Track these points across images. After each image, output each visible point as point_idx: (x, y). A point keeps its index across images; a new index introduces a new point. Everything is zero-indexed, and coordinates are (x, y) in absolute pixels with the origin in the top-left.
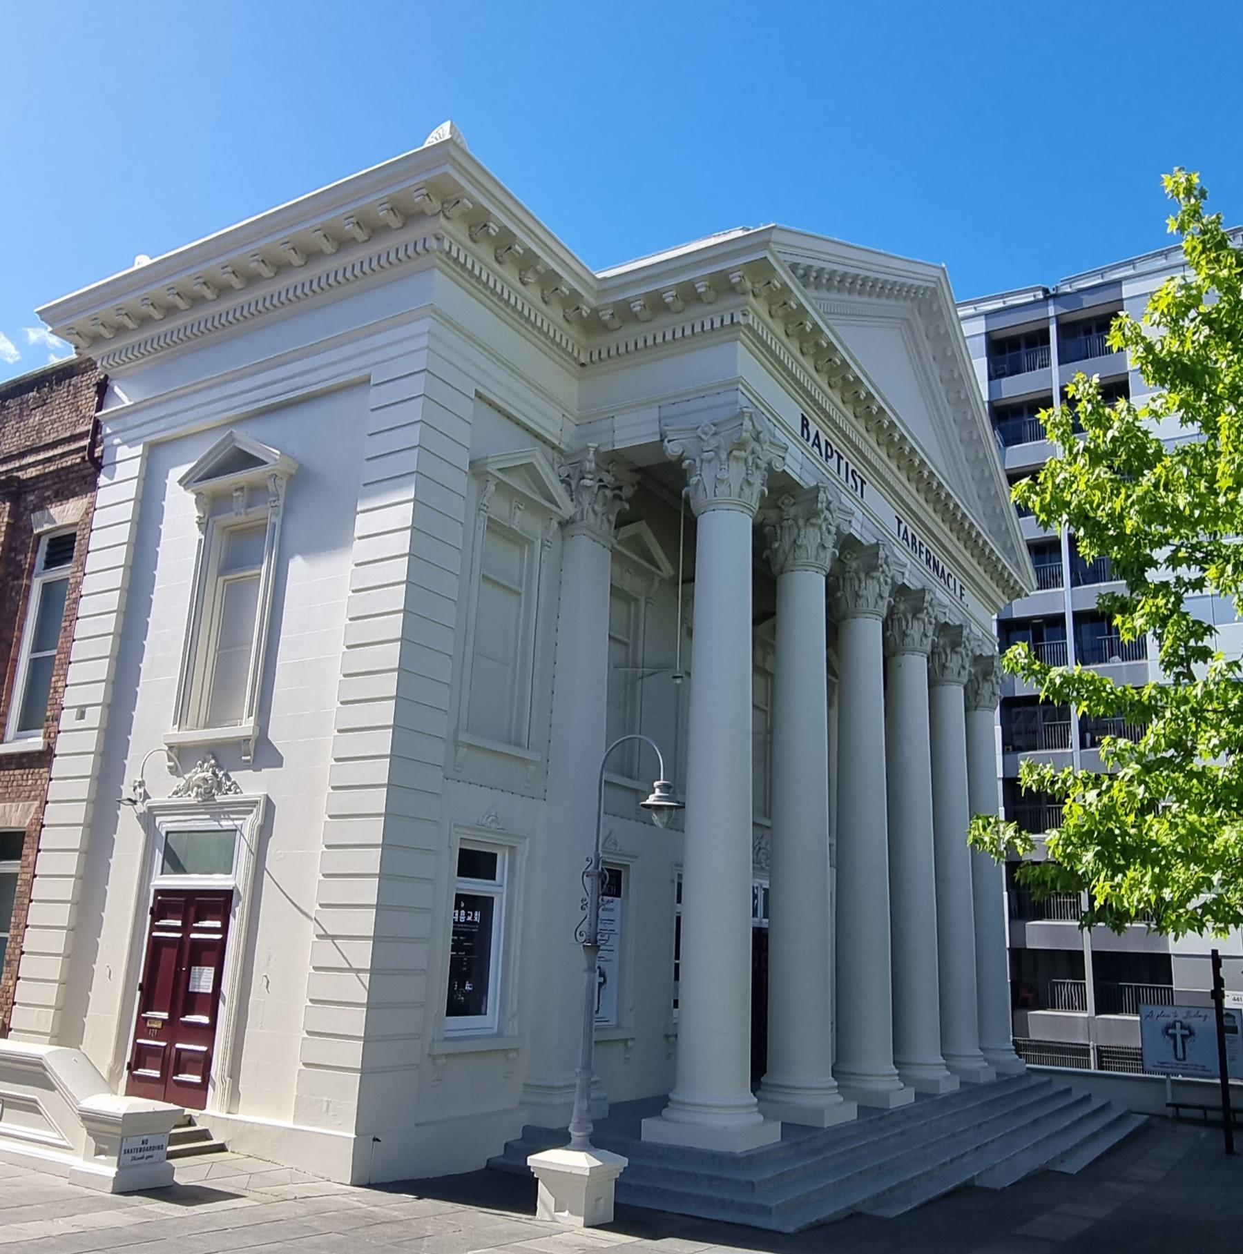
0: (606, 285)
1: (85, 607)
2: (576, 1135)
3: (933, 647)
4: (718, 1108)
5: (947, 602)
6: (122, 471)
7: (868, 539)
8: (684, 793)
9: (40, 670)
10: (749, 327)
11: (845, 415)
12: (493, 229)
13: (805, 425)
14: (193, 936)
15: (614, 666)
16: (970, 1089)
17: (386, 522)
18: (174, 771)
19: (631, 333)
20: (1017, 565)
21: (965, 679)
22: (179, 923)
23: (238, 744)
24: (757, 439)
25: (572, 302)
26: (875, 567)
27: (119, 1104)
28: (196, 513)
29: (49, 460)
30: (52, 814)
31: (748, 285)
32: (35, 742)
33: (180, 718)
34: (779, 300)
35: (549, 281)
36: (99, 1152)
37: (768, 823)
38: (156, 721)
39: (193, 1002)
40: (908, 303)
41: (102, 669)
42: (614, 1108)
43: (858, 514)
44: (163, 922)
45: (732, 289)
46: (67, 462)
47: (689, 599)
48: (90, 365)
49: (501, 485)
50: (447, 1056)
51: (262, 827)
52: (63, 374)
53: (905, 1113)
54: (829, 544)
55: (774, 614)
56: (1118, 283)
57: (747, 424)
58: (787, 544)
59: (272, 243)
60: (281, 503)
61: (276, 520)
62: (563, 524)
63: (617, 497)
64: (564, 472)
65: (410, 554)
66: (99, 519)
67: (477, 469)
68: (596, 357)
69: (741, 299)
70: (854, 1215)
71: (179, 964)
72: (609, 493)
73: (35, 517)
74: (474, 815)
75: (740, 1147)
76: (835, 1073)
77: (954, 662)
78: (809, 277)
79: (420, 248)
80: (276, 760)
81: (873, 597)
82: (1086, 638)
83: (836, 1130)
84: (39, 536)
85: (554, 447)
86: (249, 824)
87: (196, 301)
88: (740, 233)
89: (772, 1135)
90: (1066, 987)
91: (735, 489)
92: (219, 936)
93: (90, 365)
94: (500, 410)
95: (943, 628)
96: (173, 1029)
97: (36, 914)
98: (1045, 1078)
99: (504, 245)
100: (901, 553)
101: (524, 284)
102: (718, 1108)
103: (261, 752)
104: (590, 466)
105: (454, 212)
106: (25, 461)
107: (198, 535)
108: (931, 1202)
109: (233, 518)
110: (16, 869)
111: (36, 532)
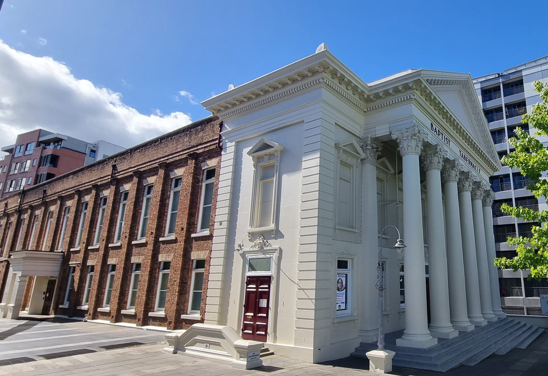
0: (372, 88)
1: (220, 191)
3: (459, 179)
4: (418, 335)
5: (476, 175)
6: (229, 150)
7: (452, 158)
9: (207, 211)
10: (415, 99)
11: (443, 122)
12: (339, 75)
16: (490, 324)
17: (311, 163)
18: (251, 240)
19: (378, 102)
20: (496, 162)
21: (482, 198)
22: (254, 286)
24: (419, 133)
25: (362, 94)
28: (252, 163)
29: (206, 147)
30: (213, 254)
31: (415, 87)
32: (206, 232)
33: (251, 225)
34: (424, 91)
35: (355, 89)
36: (241, 357)
38: (244, 226)
39: (261, 310)
41: (226, 210)
43: (449, 151)
44: (250, 286)
45: (410, 88)
46: (212, 147)
49: (344, 151)
50: (337, 323)
51: (279, 257)
52: (209, 121)
53: (472, 333)
54: (441, 162)
56: (521, 71)
57: (416, 129)
58: (447, 175)
59: (272, 82)
60: (279, 159)
61: (278, 164)
62: (362, 160)
63: (377, 151)
64: (361, 144)
65: (319, 174)
66: (222, 165)
67: (337, 146)
68: (369, 110)
69: (413, 91)
70: (461, 366)
72: (375, 150)
73: (202, 164)
74: (342, 249)
75: (426, 346)
76: (452, 322)
77: (478, 193)
78: (431, 82)
79: (317, 82)
80: (282, 236)
81: (454, 175)
82: (517, 181)
83: (453, 339)
84: (204, 170)
85: (358, 137)
86: (275, 256)
87: (250, 99)
88: (410, 71)
89: (435, 342)
91: (414, 148)
94: (342, 128)
95: (475, 183)
97: (210, 285)
99: (342, 79)
100: (461, 161)
102: (418, 335)
103: (277, 234)
105: (327, 71)
106: (198, 148)
108: (483, 360)
110: (203, 271)
111: (203, 169)
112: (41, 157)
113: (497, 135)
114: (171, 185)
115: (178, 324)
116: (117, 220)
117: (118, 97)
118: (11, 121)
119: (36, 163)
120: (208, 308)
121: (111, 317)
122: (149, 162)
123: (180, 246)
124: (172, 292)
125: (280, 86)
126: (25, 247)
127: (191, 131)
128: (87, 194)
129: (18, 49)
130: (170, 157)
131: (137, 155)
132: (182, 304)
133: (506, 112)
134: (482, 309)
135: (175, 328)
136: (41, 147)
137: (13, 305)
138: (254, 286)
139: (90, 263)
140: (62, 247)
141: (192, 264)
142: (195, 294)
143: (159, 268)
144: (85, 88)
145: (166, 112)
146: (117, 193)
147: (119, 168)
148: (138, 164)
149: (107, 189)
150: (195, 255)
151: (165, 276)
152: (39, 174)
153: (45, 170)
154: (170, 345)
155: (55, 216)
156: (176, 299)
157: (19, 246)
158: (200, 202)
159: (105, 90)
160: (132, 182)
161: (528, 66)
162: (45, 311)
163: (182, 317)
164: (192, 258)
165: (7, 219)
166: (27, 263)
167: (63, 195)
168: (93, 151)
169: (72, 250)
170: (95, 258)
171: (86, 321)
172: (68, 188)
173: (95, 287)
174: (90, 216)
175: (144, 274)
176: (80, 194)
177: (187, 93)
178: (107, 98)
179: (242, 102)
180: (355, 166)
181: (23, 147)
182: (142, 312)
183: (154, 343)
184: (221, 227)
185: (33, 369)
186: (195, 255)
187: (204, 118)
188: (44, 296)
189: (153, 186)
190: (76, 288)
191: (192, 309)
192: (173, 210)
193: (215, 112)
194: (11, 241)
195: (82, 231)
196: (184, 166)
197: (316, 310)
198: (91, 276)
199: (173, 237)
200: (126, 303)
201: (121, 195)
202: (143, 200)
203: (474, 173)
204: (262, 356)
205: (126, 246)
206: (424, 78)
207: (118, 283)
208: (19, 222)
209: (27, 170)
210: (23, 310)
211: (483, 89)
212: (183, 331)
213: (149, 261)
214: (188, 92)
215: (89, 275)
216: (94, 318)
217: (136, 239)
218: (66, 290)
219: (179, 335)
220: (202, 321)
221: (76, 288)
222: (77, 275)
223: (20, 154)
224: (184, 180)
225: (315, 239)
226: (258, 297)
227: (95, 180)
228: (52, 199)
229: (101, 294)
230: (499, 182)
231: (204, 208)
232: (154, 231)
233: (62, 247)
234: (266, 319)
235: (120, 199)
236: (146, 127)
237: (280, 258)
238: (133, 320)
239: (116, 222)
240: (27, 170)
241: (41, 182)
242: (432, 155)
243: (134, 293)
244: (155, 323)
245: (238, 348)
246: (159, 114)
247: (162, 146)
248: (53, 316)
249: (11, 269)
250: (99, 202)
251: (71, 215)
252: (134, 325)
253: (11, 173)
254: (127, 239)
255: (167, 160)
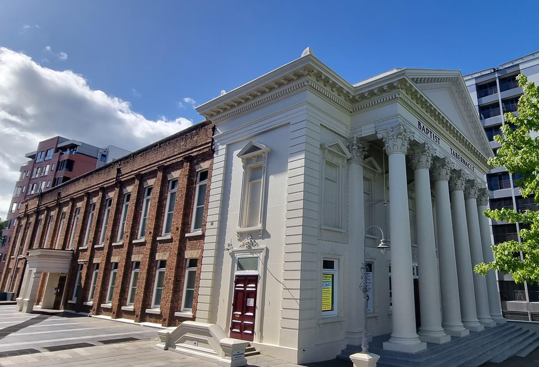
1: (212, 192)
2: (364, 349)
3: (451, 178)
6: (220, 153)
8: (389, 238)
10: (400, 98)
11: (432, 120)
12: (323, 77)
13: (419, 124)
14: (247, 289)
15: (366, 201)
16: (488, 329)
17: (297, 164)
19: (365, 102)
21: (476, 197)
22: (243, 285)
23: (258, 231)
24: (405, 132)
25: (347, 95)
26: (445, 165)
27: (232, 342)
28: (242, 164)
29: (200, 150)
30: (205, 254)
32: (199, 232)
33: (240, 225)
34: (409, 89)
35: (340, 90)
37: (416, 246)
39: (249, 309)
40: (450, 82)
42: (374, 338)
45: (395, 88)
46: (205, 150)
47: (387, 179)
48: (210, 122)
49: (330, 151)
52: (203, 125)
53: (467, 338)
54: (430, 160)
55: (413, 180)
56: (518, 65)
57: (402, 128)
58: (416, 161)
59: (260, 86)
61: (265, 165)
62: (348, 160)
64: (347, 144)
66: (215, 166)
67: (322, 147)
68: (355, 110)
71: (244, 298)
72: (361, 150)
73: (196, 167)
74: (327, 250)
75: (414, 351)
77: (472, 191)
78: (416, 81)
80: (269, 236)
81: (445, 174)
83: (444, 344)
84: (198, 172)
85: (344, 137)
86: (262, 256)
88: (395, 71)
90: (519, 293)
91: (399, 147)
92: (254, 289)
93: (210, 122)
94: (327, 128)
95: (468, 181)
96: (243, 317)
97: (202, 283)
98: (513, 325)
99: (326, 81)
100: (453, 160)
101: (333, 91)
103: (264, 234)
104: (355, 142)
105: (312, 74)
107: (243, 170)
109: (252, 165)
110: (196, 270)
112: (59, 162)
113: (494, 131)
114: (168, 186)
115: (172, 321)
116: (120, 220)
117: (127, 106)
118: (33, 129)
119: (54, 167)
120: (199, 307)
121: (112, 313)
122: (149, 165)
123: (175, 245)
124: (164, 289)
125: (267, 90)
126: (41, 246)
127: (186, 136)
128: (95, 196)
129: (43, 66)
130: (168, 160)
131: (139, 159)
132: (176, 302)
133: (503, 108)
134: (478, 313)
135: (169, 325)
136: (59, 153)
137: (28, 300)
138: (243, 285)
139: (95, 261)
140: (72, 246)
141: (186, 263)
142: (187, 291)
143: (156, 267)
144: (99, 97)
145: (171, 118)
146: (121, 195)
147: (123, 172)
148: (140, 167)
149: (113, 191)
150: (189, 254)
151: (161, 274)
152: (57, 177)
153: (61, 174)
154: (162, 342)
155: (67, 216)
156: (170, 296)
157: (36, 245)
158: (194, 202)
159: (116, 99)
160: (134, 185)
161: (525, 60)
162: (56, 306)
163: (146, 312)
164: (186, 257)
165: (27, 219)
166: (41, 261)
167: (75, 197)
168: (104, 156)
169: (80, 248)
170: (100, 256)
171: (91, 317)
172: (79, 190)
173: (99, 284)
174: (97, 217)
175: (143, 272)
176: (89, 195)
177: (190, 99)
178: (118, 106)
179: (232, 106)
180: (341, 166)
181: (43, 153)
182: (140, 309)
183: (149, 339)
184: (212, 227)
185: (37, 360)
186: (189, 254)
187: (198, 123)
188: (56, 291)
189: (152, 188)
190: (83, 285)
191: (156, 304)
192: (170, 210)
193: (208, 117)
194: (30, 239)
195: (90, 230)
196: (180, 169)
197: (300, 310)
198: (97, 273)
199: (169, 237)
200: (126, 300)
201: (124, 197)
202: (143, 201)
203: (467, 171)
204: (246, 355)
205: (127, 245)
206: (409, 77)
207: (119, 280)
208: (37, 222)
209: (46, 174)
210: (38, 304)
211: (478, 85)
212: (174, 328)
213: (148, 259)
214: (192, 98)
215: (112, 273)
216: (97, 314)
217: (136, 239)
218: (74, 287)
219: (171, 332)
220: (193, 319)
221: (83, 285)
222: (84, 272)
223: (41, 160)
224: (180, 182)
225: (299, 239)
226: (245, 296)
227: (102, 183)
228: (65, 200)
229: (105, 291)
230: (496, 180)
231: (198, 209)
232: (152, 231)
233: (72, 246)
234: (253, 318)
235: (123, 200)
236: (150, 131)
237: (266, 257)
238: (132, 317)
239: (119, 222)
240: (46, 174)
241: (58, 184)
242: (420, 154)
243: (133, 290)
244: (152, 319)
245: (224, 347)
246: (164, 120)
247: (161, 150)
248: (62, 311)
249: (28, 266)
250: (105, 202)
251: (81, 216)
252: (132, 321)
253: (33, 177)
254: (128, 238)
255: (165, 163)
